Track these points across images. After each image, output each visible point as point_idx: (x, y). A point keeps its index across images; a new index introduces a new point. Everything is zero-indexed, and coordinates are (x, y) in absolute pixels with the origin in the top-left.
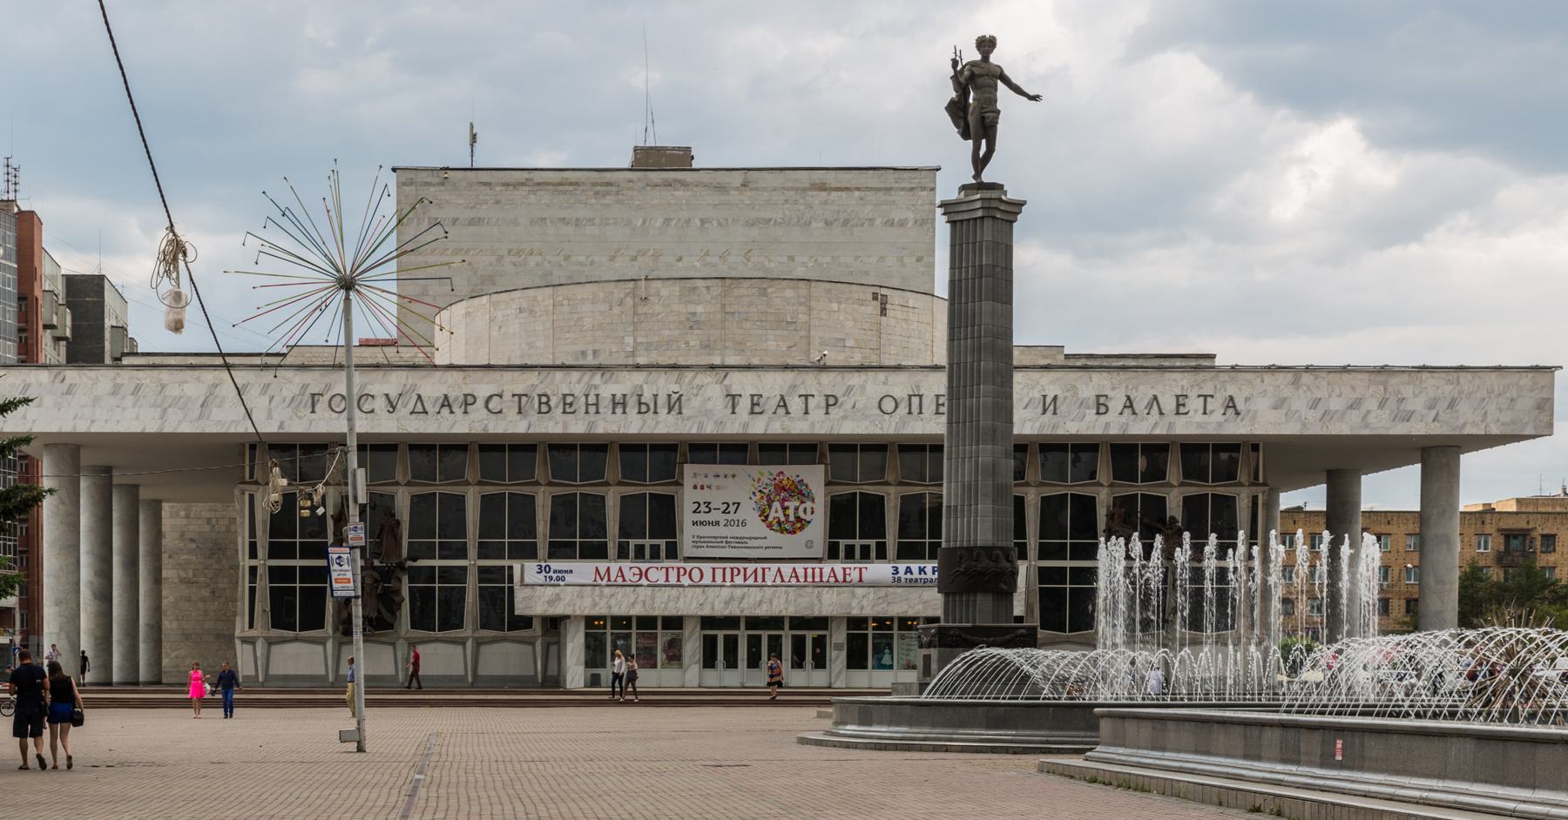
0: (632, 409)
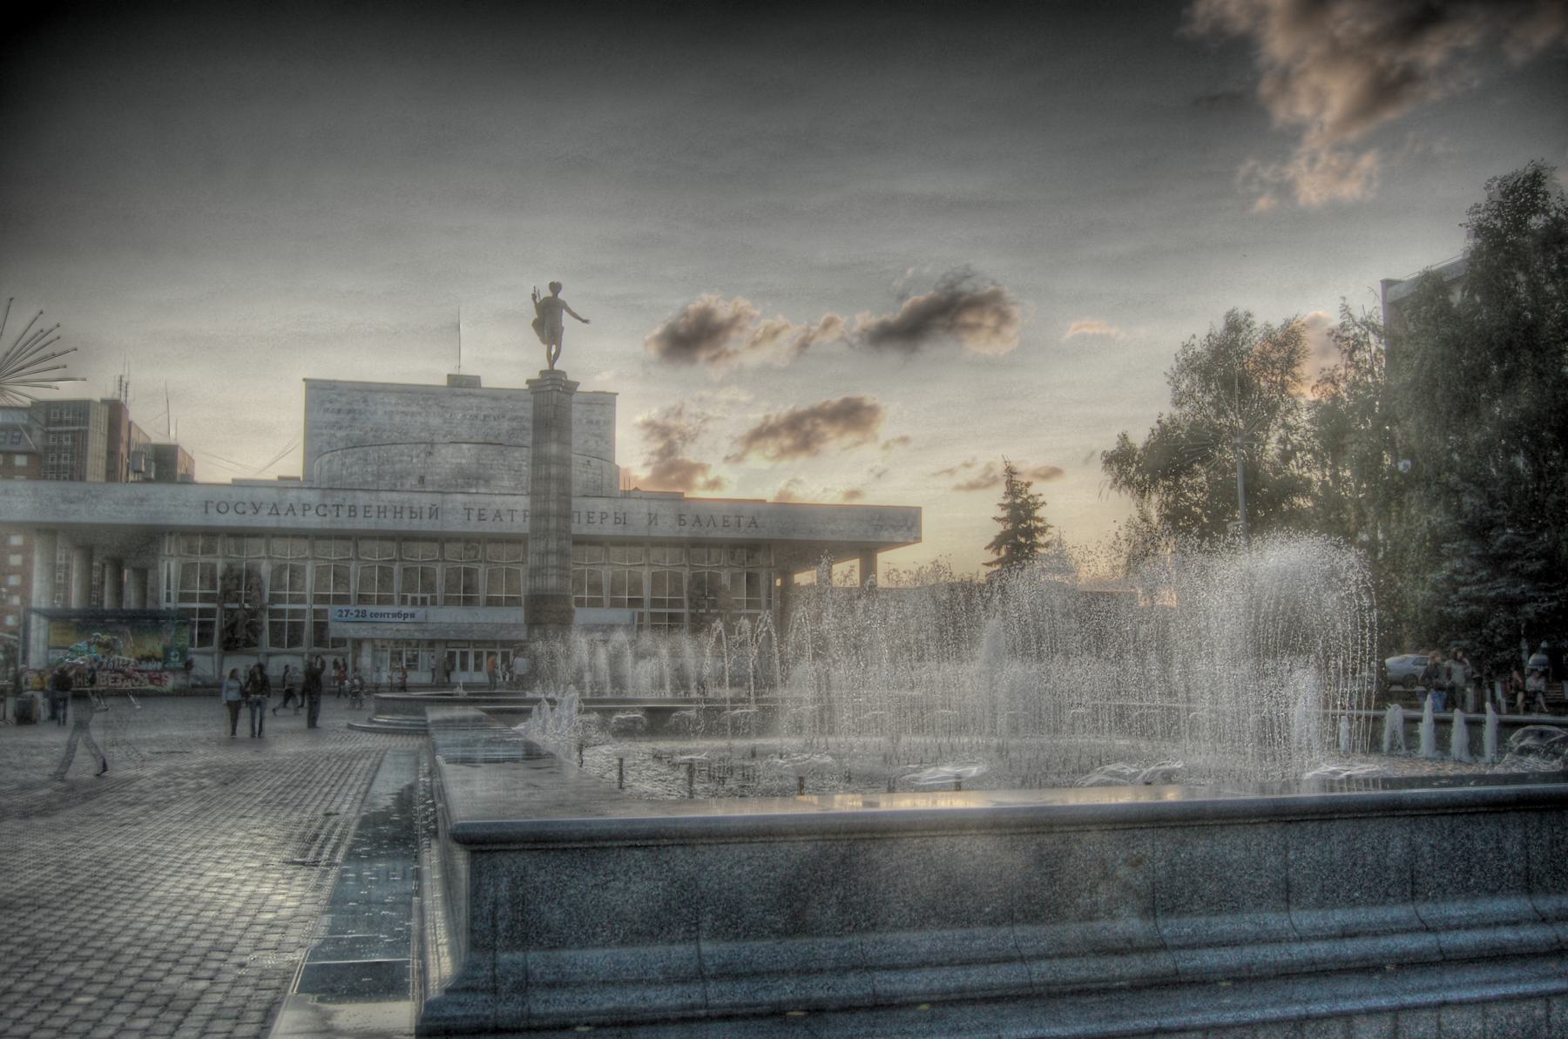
0: (406, 515)
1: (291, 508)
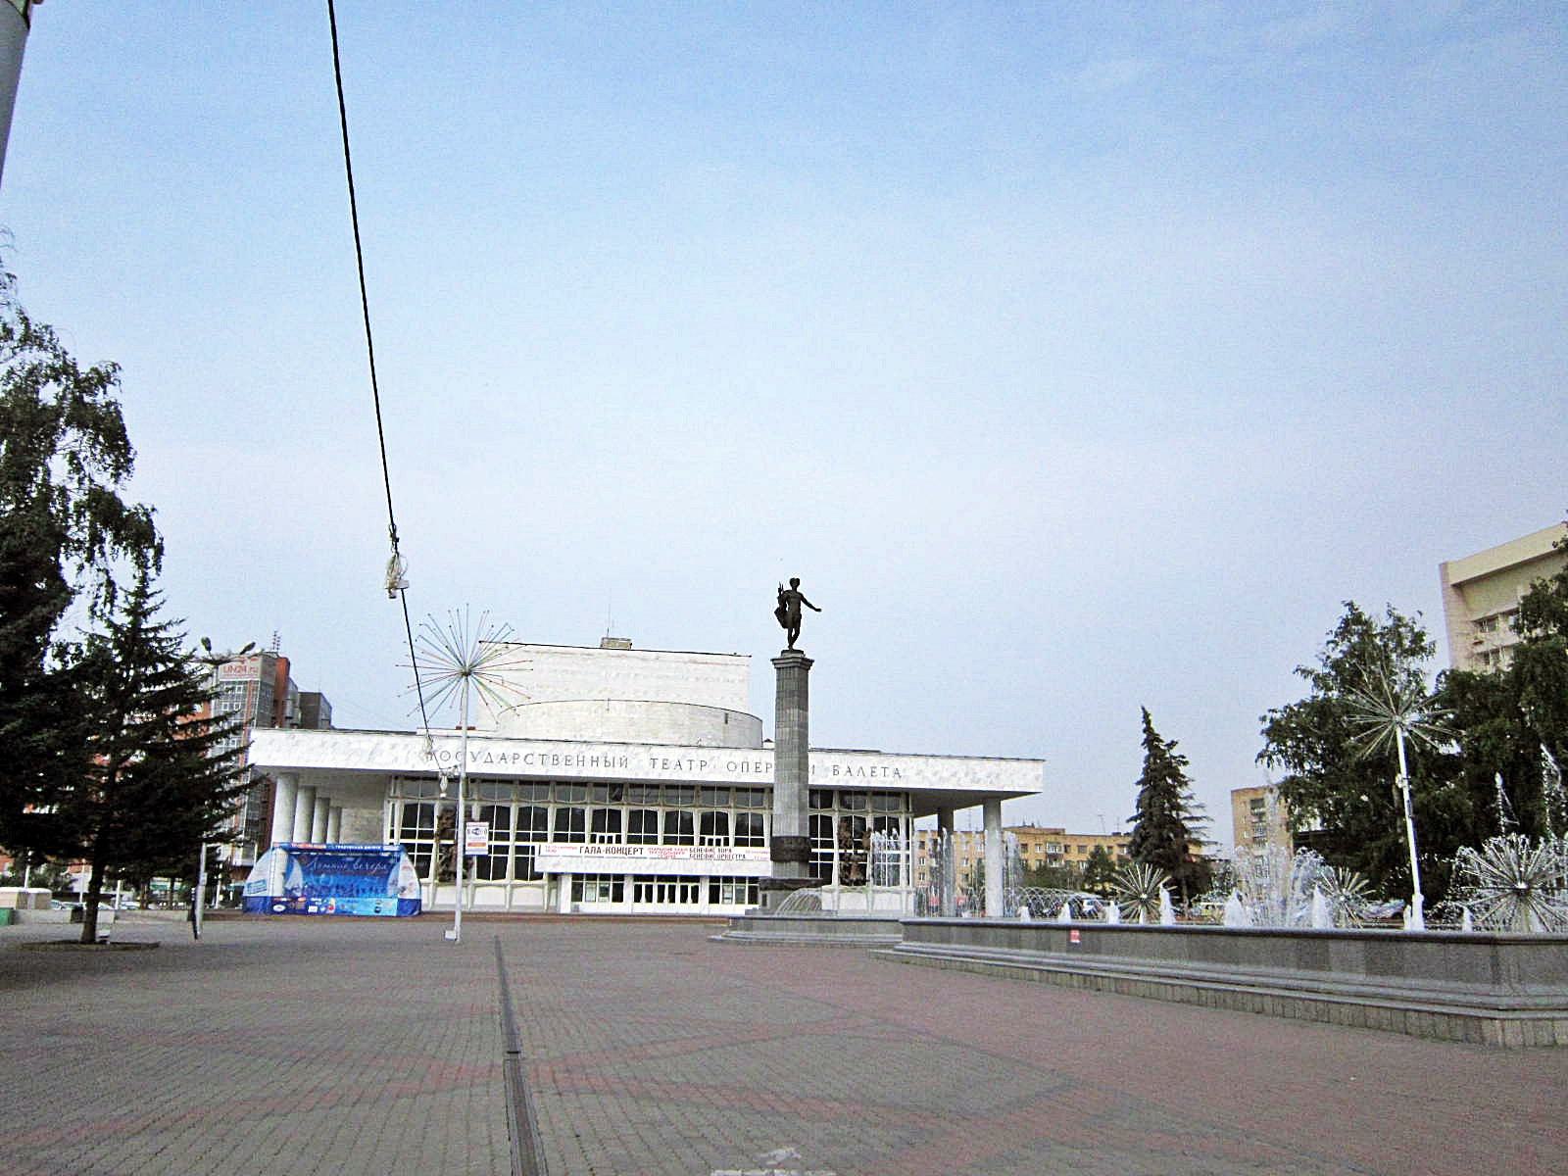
1: (503, 758)
